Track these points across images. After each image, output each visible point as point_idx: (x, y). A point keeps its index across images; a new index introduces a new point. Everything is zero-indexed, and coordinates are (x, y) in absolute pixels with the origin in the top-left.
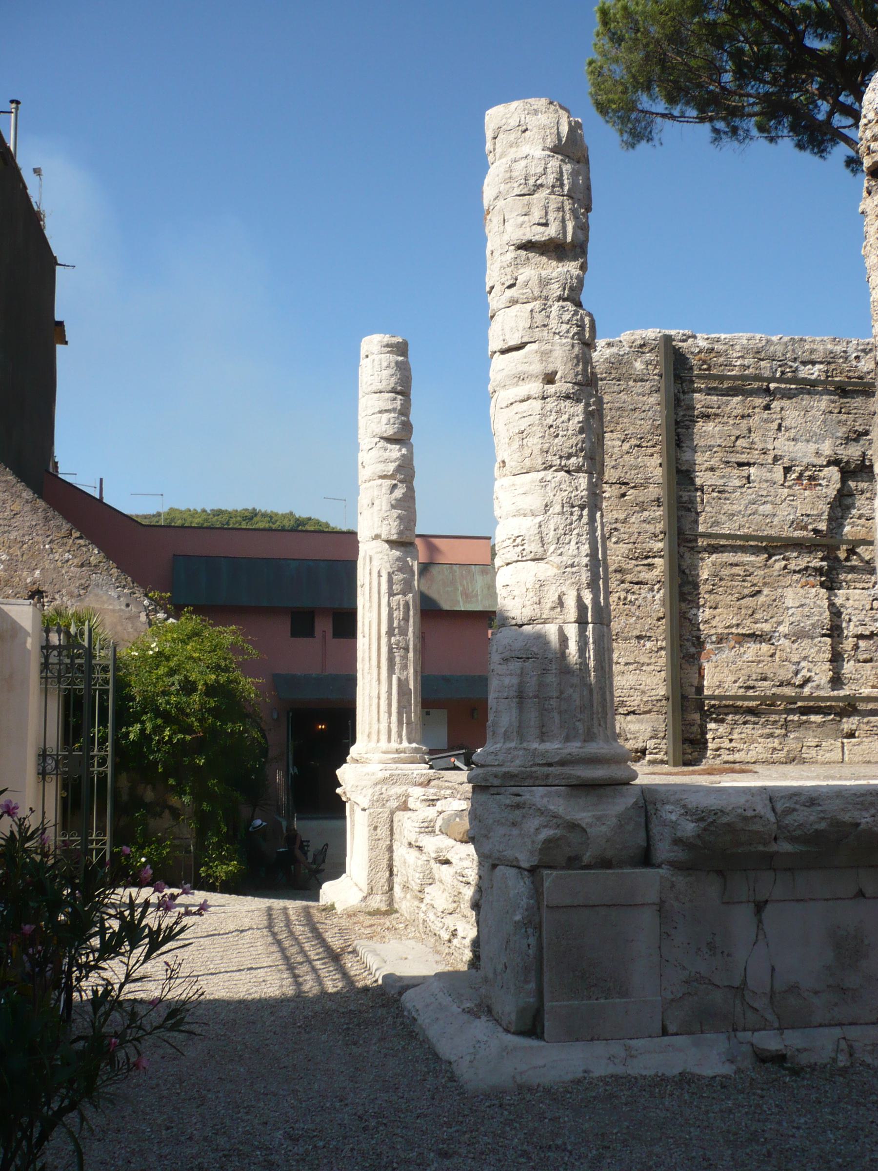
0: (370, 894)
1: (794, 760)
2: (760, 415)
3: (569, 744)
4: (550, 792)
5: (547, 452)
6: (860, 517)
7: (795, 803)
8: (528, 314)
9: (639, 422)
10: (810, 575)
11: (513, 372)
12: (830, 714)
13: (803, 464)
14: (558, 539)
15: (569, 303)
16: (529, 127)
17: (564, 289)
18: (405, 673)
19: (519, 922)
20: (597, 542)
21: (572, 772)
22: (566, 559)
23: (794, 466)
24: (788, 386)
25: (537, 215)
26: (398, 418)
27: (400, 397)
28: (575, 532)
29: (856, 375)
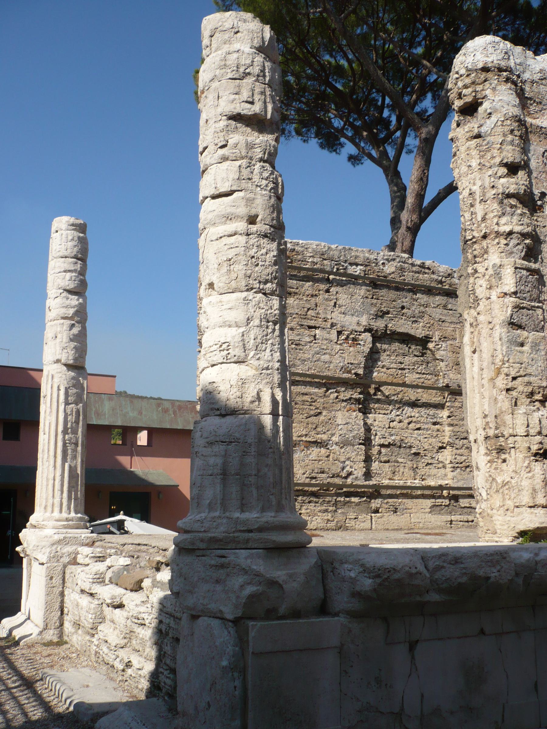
0: (45, 629)
1: (340, 528)
2: (323, 296)
3: (265, 514)
4: (252, 554)
5: (249, 277)
6: (383, 367)
7: (444, 562)
8: (237, 169)
10: (352, 403)
11: (222, 213)
12: (364, 497)
13: (349, 330)
14: (257, 347)
15: (268, 165)
16: (240, 30)
17: (265, 153)
18: (75, 462)
19: (226, 667)
20: (286, 351)
21: (269, 537)
22: (263, 363)
23: (344, 330)
24: (341, 278)
25: (245, 95)
26: (77, 277)
27: (80, 262)
28: (270, 342)
29: (383, 274)
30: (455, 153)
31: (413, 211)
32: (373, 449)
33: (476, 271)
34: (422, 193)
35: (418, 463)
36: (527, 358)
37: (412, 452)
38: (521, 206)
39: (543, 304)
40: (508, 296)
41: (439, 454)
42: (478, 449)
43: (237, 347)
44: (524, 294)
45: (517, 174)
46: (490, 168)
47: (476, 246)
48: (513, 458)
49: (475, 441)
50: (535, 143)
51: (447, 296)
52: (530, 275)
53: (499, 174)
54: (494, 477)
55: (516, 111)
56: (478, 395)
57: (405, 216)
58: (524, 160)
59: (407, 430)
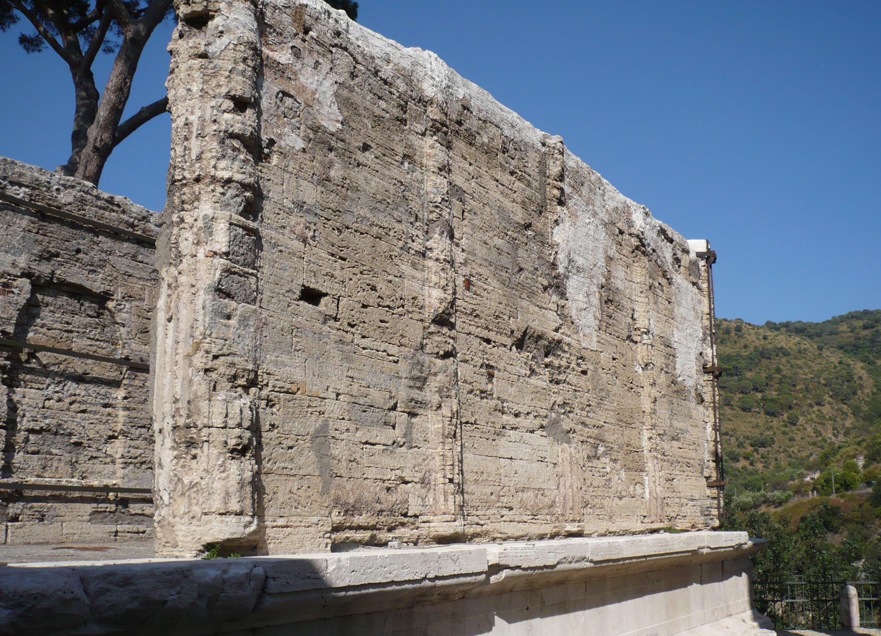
29: (55, 204)
30: (173, 70)
31: (104, 128)
32: (18, 435)
33: (182, 220)
34: (120, 107)
35: (78, 456)
36: (234, 333)
37: (72, 441)
38: (245, 150)
39: (258, 271)
40: (218, 257)
41: (107, 445)
42: (163, 441)
44: (237, 256)
45: (245, 111)
46: (214, 97)
47: (185, 189)
48: (205, 453)
49: (161, 431)
50: (269, 80)
51: (139, 244)
52: (247, 234)
53: (224, 107)
54: (180, 476)
55: (253, 37)
56: (170, 373)
57: (93, 132)
58: (254, 97)
59: (67, 412)
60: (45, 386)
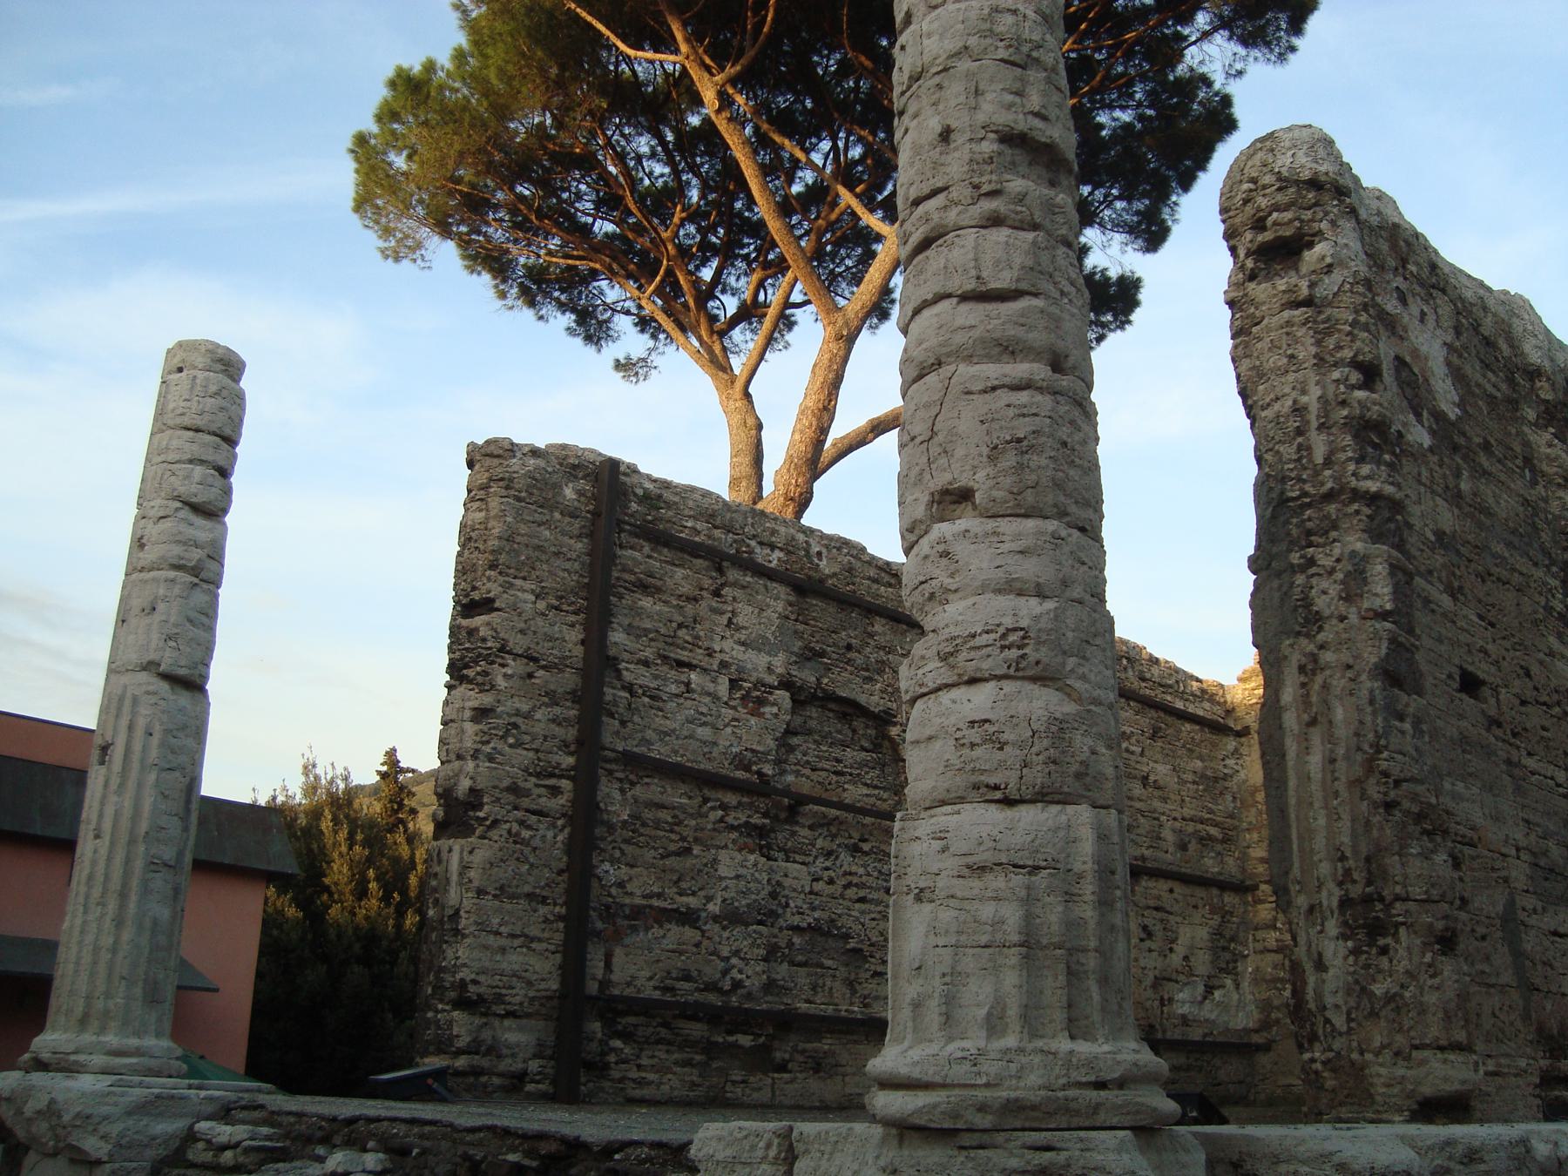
9: (561, 574)
11: (997, 335)
13: (752, 679)
21: (1139, 1100)
23: (742, 680)
33: (1312, 562)
43: (1044, 642)
46: (1334, 365)
60: (811, 859)
